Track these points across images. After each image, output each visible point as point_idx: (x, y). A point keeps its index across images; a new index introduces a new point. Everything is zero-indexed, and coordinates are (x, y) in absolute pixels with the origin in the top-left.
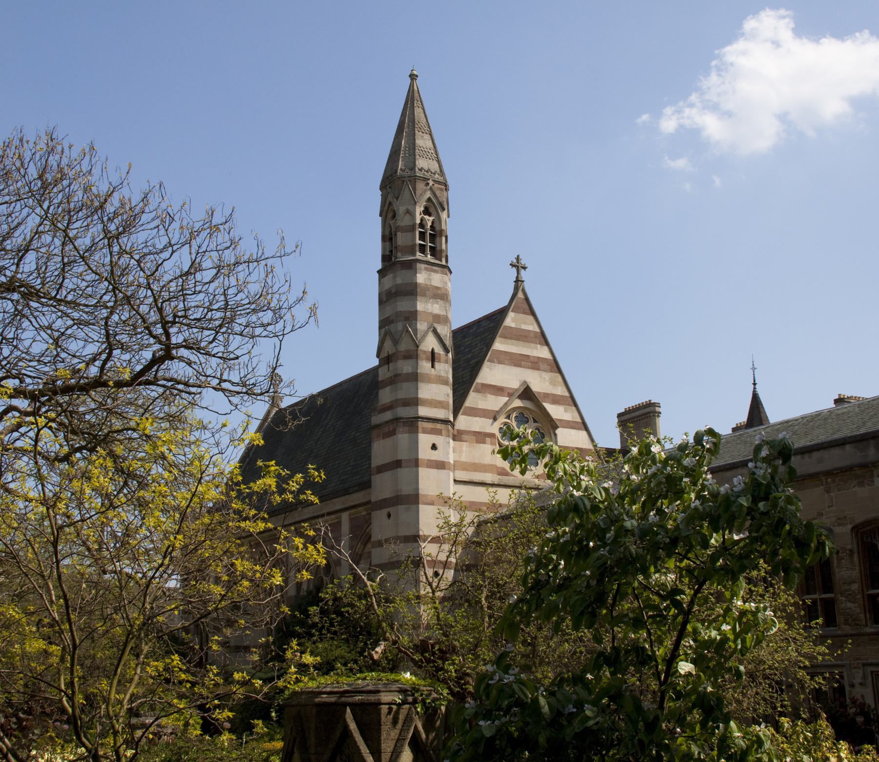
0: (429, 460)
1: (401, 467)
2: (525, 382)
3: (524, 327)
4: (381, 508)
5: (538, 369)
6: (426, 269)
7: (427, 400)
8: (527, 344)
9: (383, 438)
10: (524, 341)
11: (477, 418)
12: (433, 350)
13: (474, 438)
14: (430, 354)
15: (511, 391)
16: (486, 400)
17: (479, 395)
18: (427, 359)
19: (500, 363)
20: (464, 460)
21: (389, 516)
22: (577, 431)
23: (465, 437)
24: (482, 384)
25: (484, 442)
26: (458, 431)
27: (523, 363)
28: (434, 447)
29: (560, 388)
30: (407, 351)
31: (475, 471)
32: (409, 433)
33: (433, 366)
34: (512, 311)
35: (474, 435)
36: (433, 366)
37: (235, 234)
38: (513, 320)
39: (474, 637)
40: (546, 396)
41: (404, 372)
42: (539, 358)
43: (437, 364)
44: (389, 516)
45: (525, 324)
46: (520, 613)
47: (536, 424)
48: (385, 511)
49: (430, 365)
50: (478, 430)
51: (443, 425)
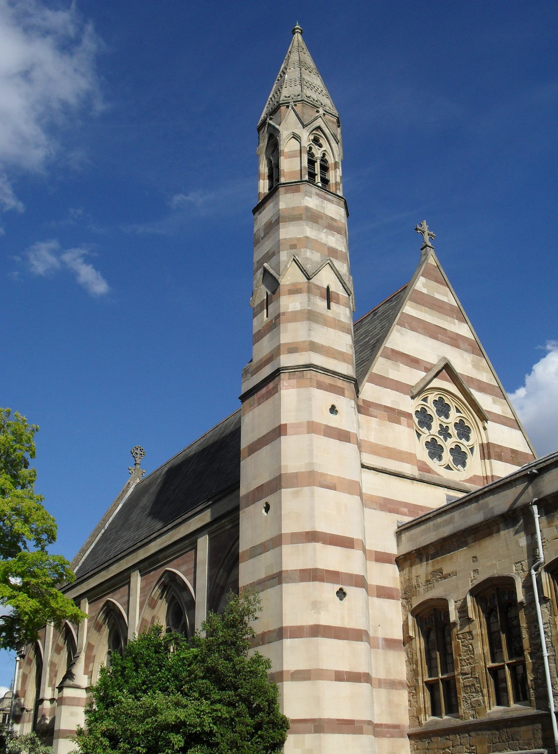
0: (327, 426)
1: (286, 435)
2: (445, 358)
3: (437, 296)
4: (254, 502)
5: (458, 347)
6: (317, 195)
7: (323, 346)
8: (442, 316)
9: (259, 404)
10: (439, 312)
11: (389, 390)
12: (328, 287)
13: (385, 414)
14: (325, 292)
15: (429, 367)
16: (398, 371)
17: (389, 363)
18: (322, 296)
19: (412, 329)
20: (373, 441)
21: (267, 508)
22: (510, 429)
23: (372, 410)
24: (393, 350)
25: (399, 422)
26: (364, 401)
27: (439, 336)
28: (333, 410)
29: (485, 374)
30: (294, 285)
31: (389, 457)
32: (298, 387)
33: (329, 307)
34: (423, 275)
35: (385, 411)
36: (329, 307)
37: (261, 605)
38: (424, 286)
39: (190, 650)
40: (471, 380)
41: (290, 310)
42: (457, 335)
43: (332, 304)
44: (267, 508)
45: (438, 293)
46: (140, 685)
47: (459, 414)
48: (261, 504)
49: (325, 304)
50: (389, 405)
51: (345, 383)
